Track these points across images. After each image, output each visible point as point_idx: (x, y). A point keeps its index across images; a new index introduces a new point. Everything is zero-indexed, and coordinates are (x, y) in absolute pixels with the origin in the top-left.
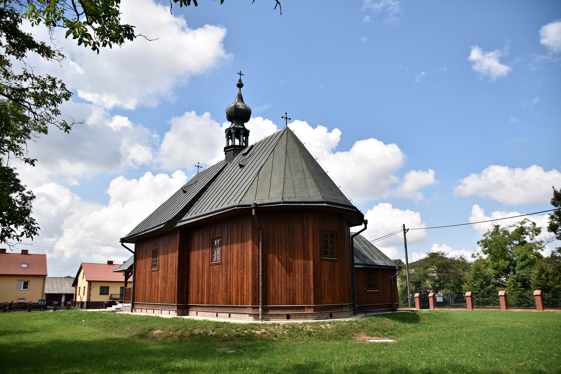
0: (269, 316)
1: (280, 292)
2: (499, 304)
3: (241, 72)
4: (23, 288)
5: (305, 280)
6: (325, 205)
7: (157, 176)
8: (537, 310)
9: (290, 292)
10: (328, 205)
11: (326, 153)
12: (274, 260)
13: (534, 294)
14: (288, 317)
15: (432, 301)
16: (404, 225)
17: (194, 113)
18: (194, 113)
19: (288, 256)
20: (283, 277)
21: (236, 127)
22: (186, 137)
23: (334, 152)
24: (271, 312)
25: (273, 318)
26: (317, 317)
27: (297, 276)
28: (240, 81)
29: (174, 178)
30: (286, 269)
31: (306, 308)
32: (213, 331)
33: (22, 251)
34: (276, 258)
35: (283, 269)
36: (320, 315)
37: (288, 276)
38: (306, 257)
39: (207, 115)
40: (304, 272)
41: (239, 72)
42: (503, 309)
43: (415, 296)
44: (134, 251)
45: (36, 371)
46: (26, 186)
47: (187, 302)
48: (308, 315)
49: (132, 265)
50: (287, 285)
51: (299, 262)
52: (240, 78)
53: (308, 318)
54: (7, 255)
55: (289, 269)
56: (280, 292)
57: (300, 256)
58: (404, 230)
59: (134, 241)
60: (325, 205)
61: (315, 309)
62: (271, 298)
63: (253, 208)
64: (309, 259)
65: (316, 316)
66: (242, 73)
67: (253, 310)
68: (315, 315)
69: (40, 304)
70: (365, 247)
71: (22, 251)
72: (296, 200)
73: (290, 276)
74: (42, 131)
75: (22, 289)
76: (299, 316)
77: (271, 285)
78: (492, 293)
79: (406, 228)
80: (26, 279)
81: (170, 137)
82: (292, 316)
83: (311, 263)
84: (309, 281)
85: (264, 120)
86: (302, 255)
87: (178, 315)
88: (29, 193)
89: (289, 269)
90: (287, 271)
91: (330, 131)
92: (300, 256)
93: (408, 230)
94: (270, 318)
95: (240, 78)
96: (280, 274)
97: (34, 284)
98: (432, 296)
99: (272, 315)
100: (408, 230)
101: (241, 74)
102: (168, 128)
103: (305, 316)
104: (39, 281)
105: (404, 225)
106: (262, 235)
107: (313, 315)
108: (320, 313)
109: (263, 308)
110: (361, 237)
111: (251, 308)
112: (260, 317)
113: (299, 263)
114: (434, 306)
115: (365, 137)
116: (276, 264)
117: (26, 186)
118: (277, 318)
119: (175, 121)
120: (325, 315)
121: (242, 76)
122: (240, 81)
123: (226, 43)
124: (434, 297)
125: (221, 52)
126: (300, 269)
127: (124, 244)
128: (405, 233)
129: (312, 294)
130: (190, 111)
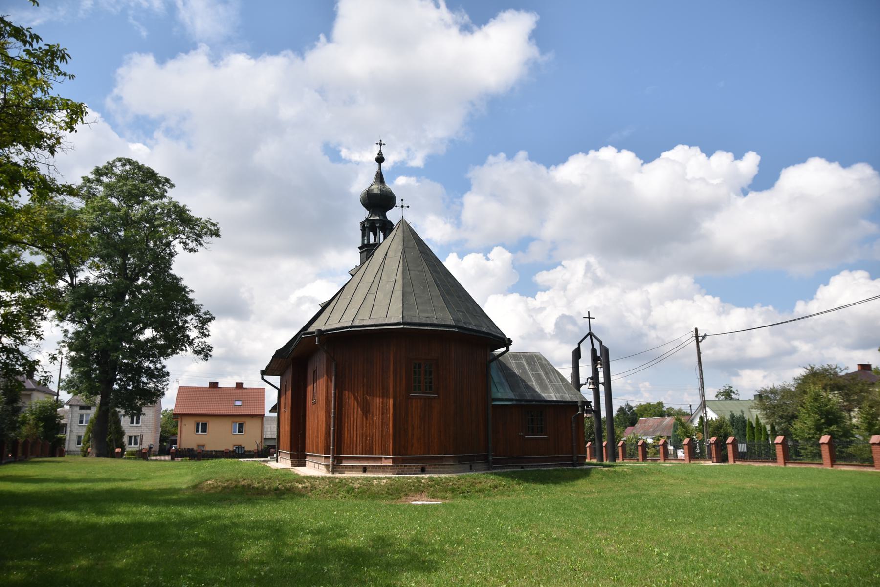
0: (342, 468)
1: (355, 439)
2: (820, 456)
3: (381, 141)
4: (202, 432)
5: (384, 423)
6: (402, 326)
7: (465, 258)
8: (877, 469)
9: (366, 439)
10: (405, 327)
11: (734, 196)
12: (349, 398)
13: (871, 442)
14: (365, 470)
15: (732, 451)
16: (696, 329)
17: (502, 155)
18: (502, 155)
19: (365, 393)
20: (359, 420)
21: (371, 219)
22: (498, 195)
23: (744, 192)
24: (345, 463)
25: (347, 471)
26: (399, 471)
27: (375, 418)
28: (380, 153)
29: (493, 260)
30: (362, 410)
31: (383, 459)
32: (258, 483)
33: (237, 384)
34: (352, 396)
35: (359, 409)
36: (404, 469)
37: (364, 419)
38: (385, 395)
39: (522, 154)
40: (382, 414)
41: (379, 142)
42: (828, 466)
43: (727, 442)
44: (279, 388)
45: (267, 538)
46: (202, 305)
47: (304, 450)
48: (387, 468)
49: (276, 405)
50: (363, 430)
51: (378, 401)
52: (380, 151)
53: (387, 472)
54: (219, 389)
55: (366, 410)
56: (355, 439)
57: (378, 395)
58: (697, 337)
59: (278, 374)
60: (402, 326)
61: (394, 460)
62: (345, 445)
63: (317, 336)
64: (388, 398)
65: (397, 470)
66: (383, 142)
67: (326, 460)
68: (397, 469)
69: (237, 452)
70: (539, 375)
71: (237, 384)
72: (387, 321)
73: (367, 419)
74: (214, 234)
75: (237, 433)
76: (377, 469)
77: (346, 429)
78: (837, 439)
79: (701, 333)
80: (241, 420)
81: (472, 200)
82: (369, 468)
83: (391, 401)
84: (388, 425)
85: (619, 151)
86: (381, 391)
87: (293, 465)
88: (205, 314)
89: (366, 410)
90: (363, 413)
91: (738, 156)
92: (378, 395)
93: (704, 337)
94: (345, 471)
95: (380, 151)
96: (356, 416)
97: (251, 427)
98: (780, 442)
99: (346, 467)
100: (704, 337)
101: (381, 144)
102: (465, 187)
103: (383, 469)
104: (256, 423)
105: (696, 329)
106: (336, 368)
107: (394, 469)
108: (405, 466)
109: (334, 458)
110: (500, 362)
111: (323, 458)
112: (330, 469)
113: (377, 402)
114: (734, 459)
115: (800, 159)
116: (351, 402)
117: (202, 305)
118: (352, 471)
119: (476, 173)
120: (412, 468)
121: (382, 146)
122: (380, 153)
123: (537, 36)
124: (734, 444)
125: (533, 51)
126: (378, 410)
127: (265, 377)
128: (698, 342)
129: (391, 441)
130: (495, 154)
